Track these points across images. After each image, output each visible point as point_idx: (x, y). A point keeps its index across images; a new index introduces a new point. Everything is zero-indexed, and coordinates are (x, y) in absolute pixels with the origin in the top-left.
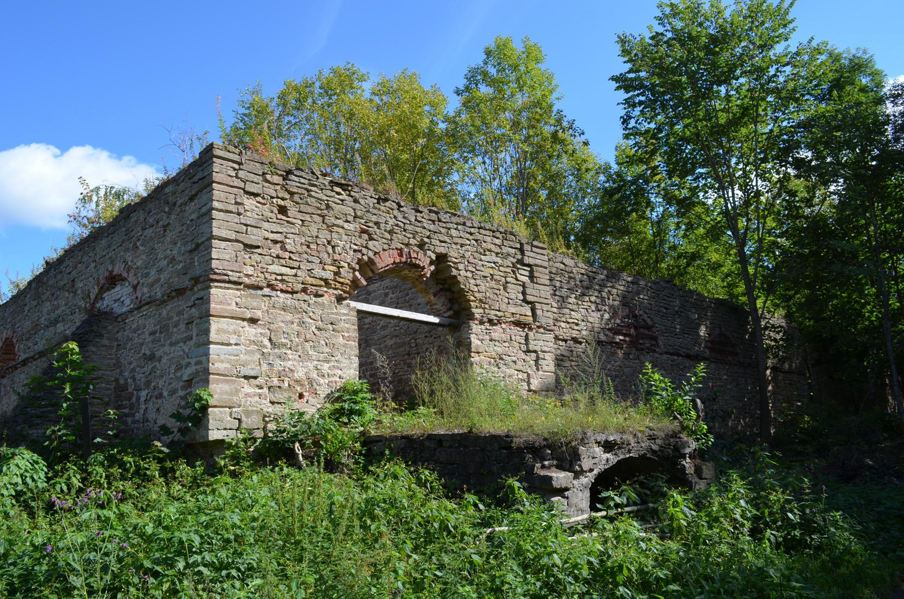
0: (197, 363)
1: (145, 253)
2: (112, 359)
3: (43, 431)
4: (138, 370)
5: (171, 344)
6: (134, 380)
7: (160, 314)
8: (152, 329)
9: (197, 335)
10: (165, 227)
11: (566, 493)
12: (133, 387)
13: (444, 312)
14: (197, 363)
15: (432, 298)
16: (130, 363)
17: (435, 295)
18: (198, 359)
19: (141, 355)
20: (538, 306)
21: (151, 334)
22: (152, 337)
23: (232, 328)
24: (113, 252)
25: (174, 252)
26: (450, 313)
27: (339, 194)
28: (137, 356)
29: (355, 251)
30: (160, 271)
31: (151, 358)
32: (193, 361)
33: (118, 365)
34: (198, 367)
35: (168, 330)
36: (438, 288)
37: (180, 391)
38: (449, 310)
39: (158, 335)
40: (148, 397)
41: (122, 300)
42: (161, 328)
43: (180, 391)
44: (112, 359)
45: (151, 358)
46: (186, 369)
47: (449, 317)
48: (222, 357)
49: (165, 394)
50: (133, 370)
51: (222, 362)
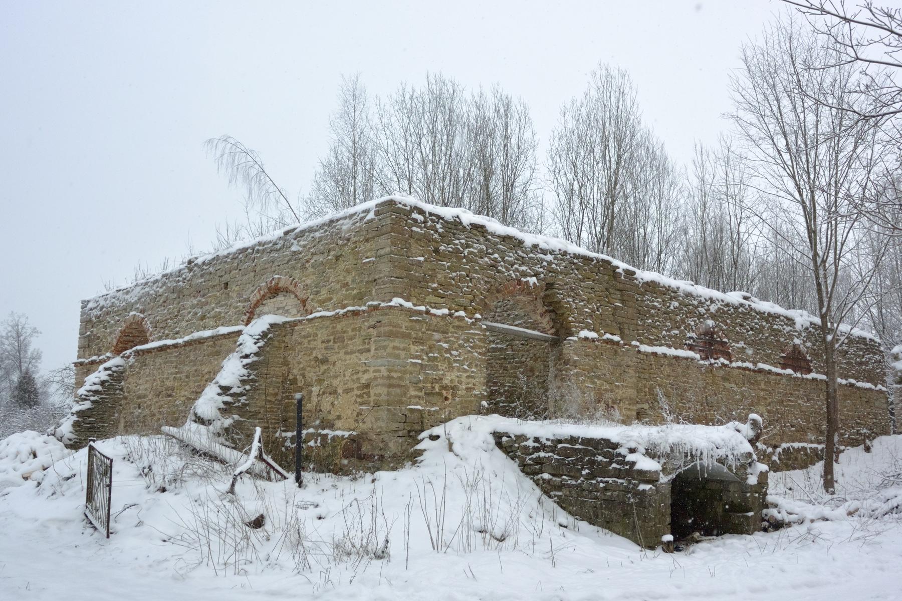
0: (374, 371)
1: (315, 274)
2: (280, 357)
3: (796, 434)
4: (308, 369)
5: (347, 353)
6: (304, 376)
7: (334, 328)
8: (325, 338)
9: (376, 349)
10: (337, 258)
11: (805, 98)
12: (303, 383)
13: (548, 330)
14: (374, 371)
15: (539, 318)
16: (299, 363)
17: (542, 315)
18: (376, 368)
19: (312, 357)
20: (626, 327)
21: (323, 342)
22: (324, 345)
23: (402, 346)
24: (277, 268)
25: (348, 279)
26: (553, 330)
27: (476, 235)
28: (307, 358)
29: (486, 282)
30: (331, 291)
31: (324, 361)
32: (372, 369)
33: (286, 363)
34: (377, 374)
35: (343, 341)
36: (544, 310)
37: (355, 390)
38: (551, 328)
39: (331, 343)
40: (321, 392)
41: (286, 308)
42: (334, 338)
43: (355, 390)
44: (280, 357)
45: (324, 361)
46: (363, 374)
47: (552, 334)
48: (396, 368)
49: (340, 391)
50: (304, 369)
51: (396, 371)
